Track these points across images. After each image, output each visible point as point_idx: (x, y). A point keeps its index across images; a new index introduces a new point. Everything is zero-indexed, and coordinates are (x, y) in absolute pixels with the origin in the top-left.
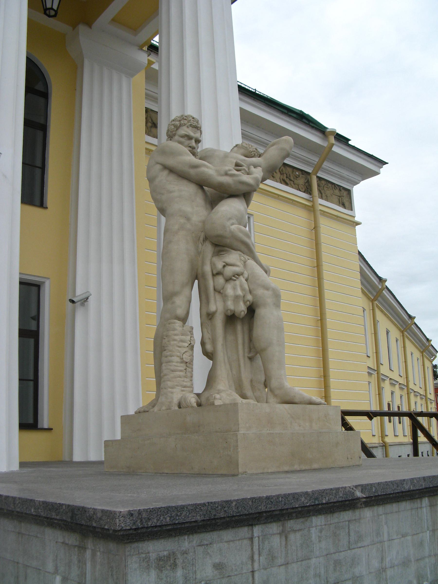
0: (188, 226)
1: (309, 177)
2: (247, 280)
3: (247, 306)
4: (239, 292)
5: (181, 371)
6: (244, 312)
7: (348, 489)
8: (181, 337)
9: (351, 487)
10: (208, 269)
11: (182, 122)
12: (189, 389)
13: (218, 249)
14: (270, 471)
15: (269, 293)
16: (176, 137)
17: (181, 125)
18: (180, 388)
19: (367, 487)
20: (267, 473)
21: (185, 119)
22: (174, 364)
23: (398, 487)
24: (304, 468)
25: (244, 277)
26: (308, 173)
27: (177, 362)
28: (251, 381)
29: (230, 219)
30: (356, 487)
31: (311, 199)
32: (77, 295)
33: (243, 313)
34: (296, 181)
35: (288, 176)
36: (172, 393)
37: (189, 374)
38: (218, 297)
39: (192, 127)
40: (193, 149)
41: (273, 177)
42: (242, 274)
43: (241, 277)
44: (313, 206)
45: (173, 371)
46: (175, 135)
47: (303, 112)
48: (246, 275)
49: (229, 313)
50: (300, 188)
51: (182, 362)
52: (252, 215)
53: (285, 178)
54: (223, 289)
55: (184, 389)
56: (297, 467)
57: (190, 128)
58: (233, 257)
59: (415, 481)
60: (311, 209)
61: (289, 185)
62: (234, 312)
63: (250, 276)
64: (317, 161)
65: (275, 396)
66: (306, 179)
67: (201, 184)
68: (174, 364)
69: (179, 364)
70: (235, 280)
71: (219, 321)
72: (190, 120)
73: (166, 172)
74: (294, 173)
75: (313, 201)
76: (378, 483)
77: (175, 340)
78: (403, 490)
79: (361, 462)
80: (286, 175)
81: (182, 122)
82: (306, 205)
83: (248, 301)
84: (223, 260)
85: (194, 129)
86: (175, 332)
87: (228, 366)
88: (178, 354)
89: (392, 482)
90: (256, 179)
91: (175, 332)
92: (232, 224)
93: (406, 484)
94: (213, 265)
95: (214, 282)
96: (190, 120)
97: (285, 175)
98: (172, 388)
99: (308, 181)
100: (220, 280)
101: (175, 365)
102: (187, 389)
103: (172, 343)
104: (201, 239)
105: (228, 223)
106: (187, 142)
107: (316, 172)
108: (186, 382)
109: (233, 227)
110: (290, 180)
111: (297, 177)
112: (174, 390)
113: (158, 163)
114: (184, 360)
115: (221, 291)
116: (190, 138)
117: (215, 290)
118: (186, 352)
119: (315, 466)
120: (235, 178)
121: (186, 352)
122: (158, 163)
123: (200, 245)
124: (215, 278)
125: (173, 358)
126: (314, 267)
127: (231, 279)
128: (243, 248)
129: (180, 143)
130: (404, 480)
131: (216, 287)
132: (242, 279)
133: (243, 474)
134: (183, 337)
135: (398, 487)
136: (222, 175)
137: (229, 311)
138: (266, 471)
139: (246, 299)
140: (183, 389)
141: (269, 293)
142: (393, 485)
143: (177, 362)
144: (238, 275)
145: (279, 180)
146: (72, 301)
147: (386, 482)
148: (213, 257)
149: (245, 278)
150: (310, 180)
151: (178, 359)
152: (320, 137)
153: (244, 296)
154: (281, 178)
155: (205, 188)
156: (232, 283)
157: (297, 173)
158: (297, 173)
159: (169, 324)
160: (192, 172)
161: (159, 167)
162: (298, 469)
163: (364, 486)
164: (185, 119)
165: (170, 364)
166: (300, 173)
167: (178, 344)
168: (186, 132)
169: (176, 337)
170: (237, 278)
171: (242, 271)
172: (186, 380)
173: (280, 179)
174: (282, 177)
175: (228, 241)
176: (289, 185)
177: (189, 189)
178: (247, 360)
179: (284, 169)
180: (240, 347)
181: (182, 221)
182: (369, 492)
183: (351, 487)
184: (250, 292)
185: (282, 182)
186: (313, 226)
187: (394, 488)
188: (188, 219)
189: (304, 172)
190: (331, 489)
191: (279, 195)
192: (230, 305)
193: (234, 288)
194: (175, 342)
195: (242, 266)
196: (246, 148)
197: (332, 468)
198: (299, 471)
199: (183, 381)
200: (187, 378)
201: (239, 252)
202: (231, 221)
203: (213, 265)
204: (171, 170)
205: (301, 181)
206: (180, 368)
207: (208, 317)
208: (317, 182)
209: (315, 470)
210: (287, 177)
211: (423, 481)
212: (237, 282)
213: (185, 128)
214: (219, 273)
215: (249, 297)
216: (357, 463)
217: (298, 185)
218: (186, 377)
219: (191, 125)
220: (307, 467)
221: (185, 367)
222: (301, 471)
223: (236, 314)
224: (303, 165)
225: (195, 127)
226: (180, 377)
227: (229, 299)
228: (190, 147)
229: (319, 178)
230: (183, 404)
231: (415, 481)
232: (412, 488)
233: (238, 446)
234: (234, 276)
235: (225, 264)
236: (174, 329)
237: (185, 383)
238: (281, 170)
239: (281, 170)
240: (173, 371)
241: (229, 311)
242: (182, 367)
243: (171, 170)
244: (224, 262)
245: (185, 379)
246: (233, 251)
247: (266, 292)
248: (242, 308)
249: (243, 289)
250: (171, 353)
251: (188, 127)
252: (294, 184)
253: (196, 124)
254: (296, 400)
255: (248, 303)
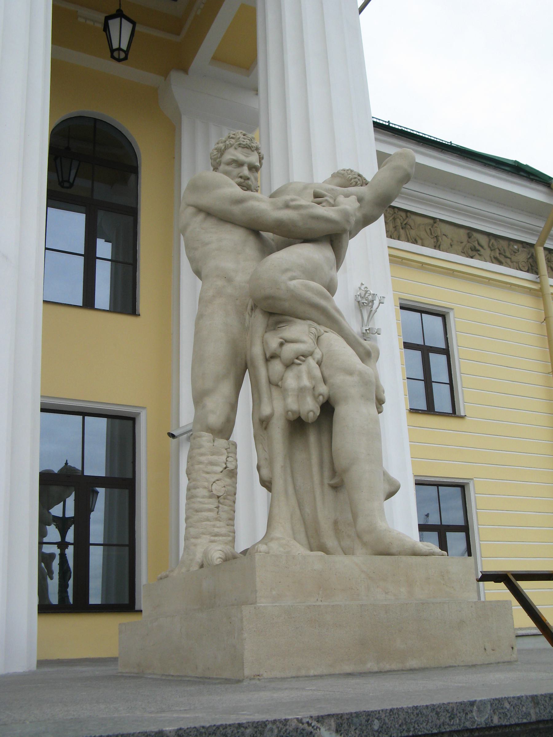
0: (229, 290)
1: (532, 250)
2: (319, 364)
3: (320, 404)
4: (306, 382)
5: (210, 510)
6: (314, 413)
7: (294, 724)
8: (210, 457)
9: (305, 721)
10: (257, 351)
11: (227, 142)
12: (224, 538)
13: (274, 319)
14: (312, 673)
15: (355, 378)
16: (222, 167)
17: (226, 148)
18: (208, 537)
19: (355, 720)
20: (306, 676)
21: (232, 138)
22: (199, 499)
23: (451, 718)
24: (387, 667)
25: (314, 359)
26: (532, 245)
27: (203, 497)
28: (336, 523)
29: (286, 270)
30: (320, 719)
31: (538, 280)
32: (181, 426)
33: (311, 414)
34: (514, 258)
35: (502, 251)
36: (195, 545)
37: (224, 515)
38: (276, 393)
39: (243, 148)
40: (245, 180)
41: (480, 255)
42: (311, 354)
43: (310, 359)
44: (541, 290)
45: (197, 511)
46: (219, 164)
47: (518, 162)
48: (318, 355)
49: (291, 417)
50: (520, 266)
51: (211, 497)
52: (452, 309)
53: (498, 255)
54: (282, 379)
55: (216, 538)
56: (371, 666)
57: (240, 149)
58: (299, 332)
59: (507, 705)
60: (539, 294)
61: (505, 264)
62: (299, 413)
63: (324, 358)
64: (543, 226)
65: (364, 544)
66: (529, 254)
67: (255, 228)
68: (199, 499)
69: (206, 500)
70: (300, 364)
71: (278, 430)
72: (239, 138)
73: (201, 216)
74: (511, 247)
75: (540, 283)
76: (391, 710)
77: (200, 463)
78: (468, 725)
79: (514, 656)
80: (499, 250)
81: (227, 142)
82: (531, 289)
83: (320, 394)
84: (280, 335)
85: (246, 150)
86: (202, 450)
87: (293, 501)
88: (206, 484)
89: (433, 708)
90: (346, 215)
91: (202, 450)
92: (292, 278)
93: (479, 711)
94: (264, 343)
95: (267, 370)
96: (239, 138)
97: (497, 250)
98: (196, 538)
99: (532, 255)
100: (277, 366)
101: (200, 502)
102: (221, 538)
103: (196, 467)
104: (249, 307)
105: (285, 277)
106: (236, 171)
107: (542, 242)
108: (218, 527)
109: (294, 284)
110: (506, 257)
111: (515, 252)
112: (199, 541)
113: (189, 205)
114: (214, 492)
115: (280, 383)
116: (240, 164)
117: (270, 382)
118: (218, 480)
119: (413, 663)
120: (303, 212)
121: (218, 480)
122: (189, 205)
123: (247, 317)
124: (269, 363)
125: (198, 490)
126: (549, 373)
127: (293, 363)
128: (315, 314)
129: (227, 173)
130: (472, 703)
131: (271, 378)
132: (312, 362)
133: (254, 679)
134: (214, 458)
135: (451, 718)
136: (281, 208)
137: (290, 413)
138: (303, 673)
139: (317, 393)
140: (213, 538)
141: (355, 378)
142: (437, 713)
143: (203, 497)
144: (304, 356)
145: (488, 258)
146: (172, 436)
147: (416, 708)
148: (266, 332)
149: (316, 360)
150: (534, 254)
151: (205, 493)
152: (544, 193)
153: (314, 388)
154: (492, 256)
155: (264, 234)
156: (295, 369)
157: (516, 247)
158: (516, 247)
159: (194, 438)
160: (236, 209)
161: (191, 210)
162: (376, 669)
163: (345, 717)
164: (232, 138)
165: (193, 500)
166: (520, 245)
167: (206, 469)
168: (234, 155)
169: (203, 459)
170: (304, 361)
171: (311, 350)
172: (218, 523)
173: (490, 257)
174: (493, 254)
175: (287, 305)
176: (505, 264)
177: (233, 237)
178: (326, 487)
179: (495, 243)
180: (315, 469)
181: (220, 283)
182: (362, 730)
183: (305, 721)
184: (325, 381)
185: (494, 260)
186: (544, 317)
187: (438, 722)
188: (229, 280)
189: (524, 244)
190: (240, 725)
191: (490, 279)
192: (292, 404)
193: (299, 377)
194: (201, 466)
195: (310, 341)
196: (343, 175)
197: (450, 667)
198: (377, 672)
199: (214, 526)
200: (220, 521)
201: (310, 322)
202: (289, 274)
203: (264, 343)
204: (209, 213)
205: (522, 257)
206: (207, 506)
207: (263, 424)
208: (545, 256)
209: (412, 670)
210: (500, 254)
211: (532, 704)
212: (303, 367)
213: (231, 150)
214: (274, 356)
215: (323, 389)
216: (506, 659)
217: (518, 263)
218: (217, 519)
219: (240, 144)
220: (394, 666)
221: (216, 504)
222: (381, 672)
223: (303, 417)
224: (528, 236)
225: (246, 147)
226: (208, 520)
227: (290, 393)
228: (241, 177)
229: (545, 249)
230: (205, 564)
231: (507, 705)
232: (496, 721)
233: (243, 629)
234: (297, 358)
235: (281, 340)
236: (200, 447)
237: (216, 530)
238: (490, 245)
239: (490, 245)
240: (197, 511)
241: (290, 413)
242: (212, 504)
243: (209, 213)
244: (281, 338)
245: (218, 522)
246: (299, 321)
247: (348, 378)
248: (310, 408)
249: (311, 377)
250: (194, 483)
251: (236, 149)
252: (512, 262)
253: (248, 142)
254: (394, 550)
255: (321, 397)
